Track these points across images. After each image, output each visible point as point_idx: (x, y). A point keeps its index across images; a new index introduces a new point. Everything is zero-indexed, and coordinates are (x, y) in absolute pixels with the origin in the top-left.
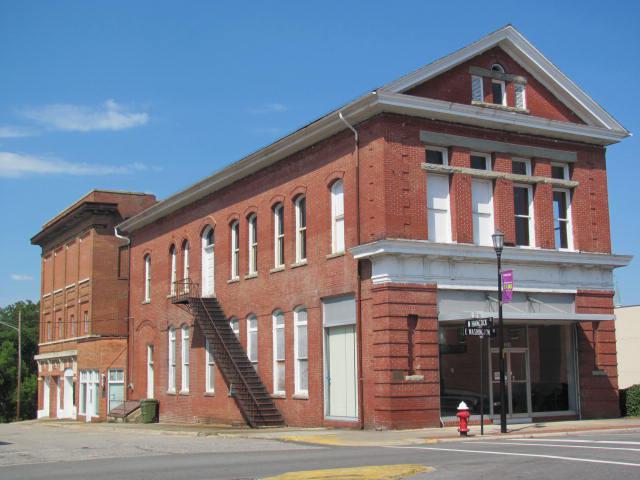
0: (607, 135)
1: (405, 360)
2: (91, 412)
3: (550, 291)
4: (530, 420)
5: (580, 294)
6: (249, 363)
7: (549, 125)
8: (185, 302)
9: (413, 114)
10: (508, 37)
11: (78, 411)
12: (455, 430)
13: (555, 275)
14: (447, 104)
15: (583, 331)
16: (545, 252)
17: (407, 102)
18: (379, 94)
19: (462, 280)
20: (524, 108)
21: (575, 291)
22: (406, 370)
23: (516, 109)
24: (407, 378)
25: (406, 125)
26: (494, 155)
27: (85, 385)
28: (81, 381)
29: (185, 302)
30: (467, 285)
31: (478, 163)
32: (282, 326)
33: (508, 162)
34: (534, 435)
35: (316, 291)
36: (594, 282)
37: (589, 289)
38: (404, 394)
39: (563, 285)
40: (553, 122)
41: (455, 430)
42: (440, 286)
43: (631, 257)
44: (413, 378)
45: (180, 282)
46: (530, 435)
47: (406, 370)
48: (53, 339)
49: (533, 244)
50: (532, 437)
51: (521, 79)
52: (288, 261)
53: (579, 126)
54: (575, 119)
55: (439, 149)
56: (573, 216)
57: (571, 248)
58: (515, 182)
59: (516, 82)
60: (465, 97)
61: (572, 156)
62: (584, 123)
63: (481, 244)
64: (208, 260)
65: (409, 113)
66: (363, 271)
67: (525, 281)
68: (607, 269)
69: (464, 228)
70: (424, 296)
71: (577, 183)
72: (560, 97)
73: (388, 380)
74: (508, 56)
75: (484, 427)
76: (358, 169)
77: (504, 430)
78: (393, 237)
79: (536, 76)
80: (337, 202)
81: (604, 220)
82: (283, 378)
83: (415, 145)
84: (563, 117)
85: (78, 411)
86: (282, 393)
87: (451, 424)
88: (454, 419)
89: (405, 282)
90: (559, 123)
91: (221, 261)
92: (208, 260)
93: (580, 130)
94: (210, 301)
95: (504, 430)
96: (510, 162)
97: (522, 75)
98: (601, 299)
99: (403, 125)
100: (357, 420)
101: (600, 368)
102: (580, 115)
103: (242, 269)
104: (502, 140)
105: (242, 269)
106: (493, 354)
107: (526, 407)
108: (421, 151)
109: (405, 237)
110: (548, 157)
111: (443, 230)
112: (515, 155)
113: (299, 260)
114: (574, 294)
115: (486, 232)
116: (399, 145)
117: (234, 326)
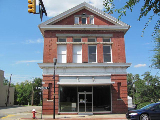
0: (122, 27)
1: (48, 96)
3: (101, 75)
4: (92, 114)
5: (112, 76)
6: (125, 104)
7: (99, 27)
9: (54, 30)
10: (86, 6)
13: (103, 70)
14: (62, 25)
15: (114, 87)
16: (99, 63)
17: (112, 27)
19: (68, 73)
20: (94, 23)
21: (111, 75)
22: (47, 99)
23: (92, 24)
24: (48, 100)
25: (52, 33)
26: (111, 37)
30: (69, 74)
31: (75, 40)
33: (87, 39)
37: (116, 74)
38: (46, 105)
39: (105, 73)
40: (100, 26)
42: (59, 75)
43: (131, 63)
44: (49, 101)
47: (47, 99)
49: (112, 62)
51: (92, 16)
53: (114, 26)
54: (113, 24)
55: (109, 38)
56: (112, 53)
57: (112, 62)
58: (88, 44)
59: (90, 17)
60: (72, 23)
61: (111, 35)
62: (115, 25)
63: (63, 63)
65: (53, 30)
67: (83, 73)
69: (70, 59)
71: (112, 43)
74: (87, 10)
75: (43, 115)
78: (45, 62)
81: (124, 53)
83: (54, 38)
84: (107, 24)
89: (48, 74)
90: (105, 26)
93: (111, 27)
96: (102, 39)
97: (93, 15)
98: (122, 77)
99: (51, 33)
101: (121, 98)
102: (114, 23)
104: (84, 33)
107: (92, 110)
108: (56, 39)
109: (49, 62)
110: (72, 36)
111: (64, 60)
112: (103, 37)
114: (110, 76)
115: (79, 60)
116: (49, 38)
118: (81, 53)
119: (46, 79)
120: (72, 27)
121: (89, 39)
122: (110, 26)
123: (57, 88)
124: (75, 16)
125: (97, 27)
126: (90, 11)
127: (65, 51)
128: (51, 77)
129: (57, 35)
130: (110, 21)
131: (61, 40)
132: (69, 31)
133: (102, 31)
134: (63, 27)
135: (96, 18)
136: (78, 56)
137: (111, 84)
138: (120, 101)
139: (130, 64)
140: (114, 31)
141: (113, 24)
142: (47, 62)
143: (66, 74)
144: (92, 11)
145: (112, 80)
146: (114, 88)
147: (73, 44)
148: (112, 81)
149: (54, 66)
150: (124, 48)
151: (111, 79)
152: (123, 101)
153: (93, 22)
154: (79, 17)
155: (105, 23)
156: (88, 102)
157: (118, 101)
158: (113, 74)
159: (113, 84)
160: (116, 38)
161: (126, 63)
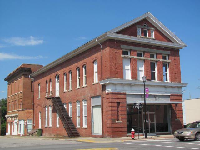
1: (116, 116)
2: (22, 133)
3: (162, 94)
5: (171, 95)
8: (50, 98)
10: (149, 16)
11: (18, 133)
12: (130, 138)
13: (164, 89)
14: (129, 36)
19: (134, 91)
20: (154, 38)
21: (170, 95)
22: (116, 119)
23: (151, 38)
24: (117, 121)
26: (144, 52)
34: (155, 139)
36: (176, 92)
39: (166, 92)
40: (163, 42)
41: (130, 138)
42: (127, 93)
45: (49, 92)
48: (11, 110)
51: (153, 29)
53: (171, 43)
54: (170, 41)
55: (127, 51)
57: (169, 81)
58: (151, 60)
59: (151, 30)
60: (135, 34)
61: (169, 53)
62: (173, 42)
64: (57, 85)
68: (180, 88)
69: (135, 75)
70: (122, 96)
71: (170, 61)
74: (148, 21)
79: (157, 28)
85: (18, 133)
86: (79, 126)
88: (131, 134)
89: (116, 92)
91: (61, 86)
95: (146, 138)
101: (178, 118)
102: (171, 40)
104: (147, 48)
108: (121, 51)
109: (116, 78)
111: (128, 75)
114: (169, 96)
118: (144, 70)
119: (114, 97)
120: (139, 39)
121: (150, 55)
122: (169, 43)
123: (125, 107)
124: (137, 26)
125: (158, 43)
126: (151, 22)
127: (129, 65)
128: (118, 95)
129: (122, 46)
130: (169, 38)
131: (125, 53)
132: (158, 47)
133: (162, 47)
134: (161, 43)
135: (156, 32)
136: (126, 71)
137: (170, 105)
138: (178, 121)
139: (186, 85)
140: (133, 42)
141: (170, 41)
142: (114, 78)
143: (133, 92)
144: (152, 23)
145: (171, 100)
146: (173, 108)
147: (138, 59)
148: (171, 101)
149: (143, 84)
150: (180, 68)
151: (169, 99)
152: (180, 121)
153: (153, 36)
154: (141, 28)
155: (164, 39)
156: (151, 122)
157: (176, 121)
158: (172, 94)
159: (172, 105)
160: (173, 56)
161: (180, 82)
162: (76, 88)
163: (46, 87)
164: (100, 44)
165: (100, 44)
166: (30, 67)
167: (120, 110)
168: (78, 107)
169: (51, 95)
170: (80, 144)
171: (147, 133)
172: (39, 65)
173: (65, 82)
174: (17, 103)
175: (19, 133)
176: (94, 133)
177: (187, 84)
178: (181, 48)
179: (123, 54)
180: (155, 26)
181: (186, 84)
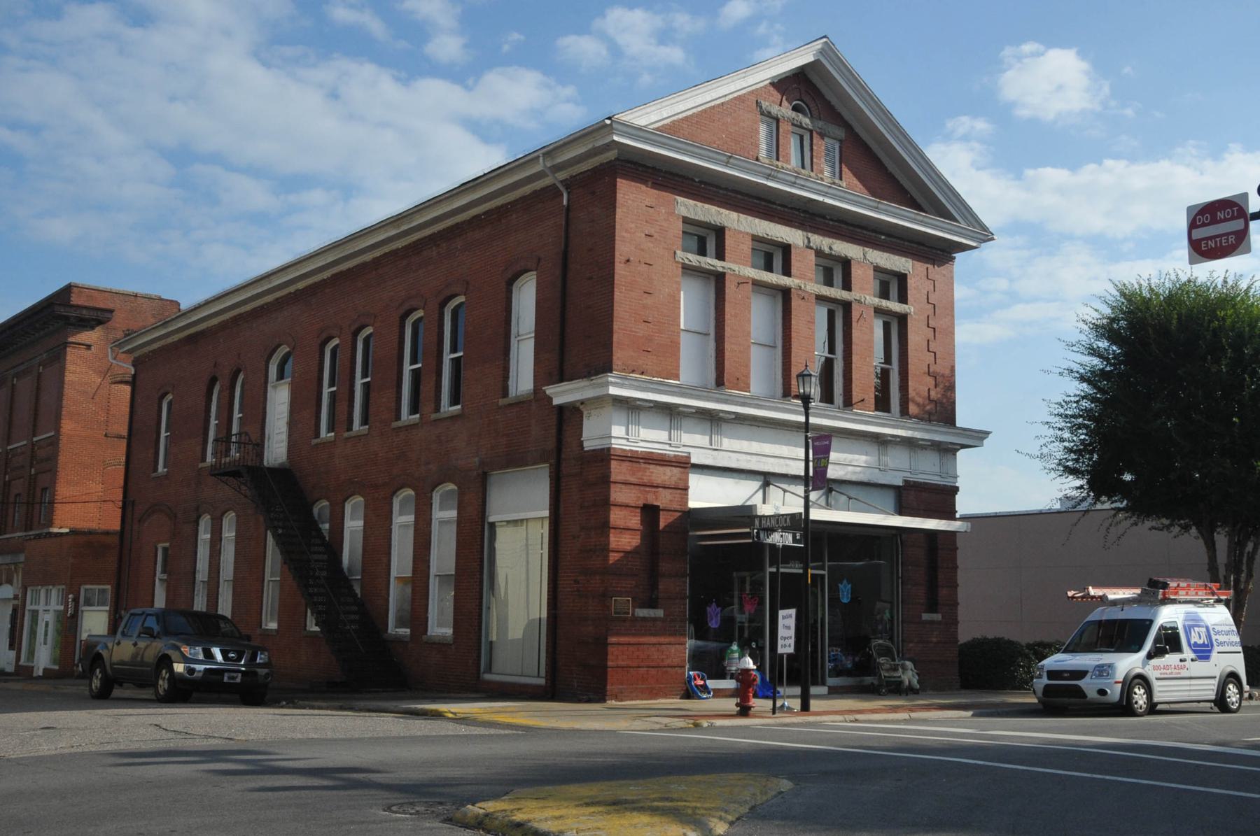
2: (43, 658)
8: (235, 474)
11: (18, 658)
12: (731, 704)
18: (615, 126)
27: (35, 614)
28: (28, 607)
29: (235, 474)
32: (410, 518)
34: (859, 717)
35: (476, 459)
36: (926, 470)
41: (731, 704)
45: (224, 440)
46: (852, 717)
48: (28, 527)
50: (856, 721)
52: (427, 407)
64: (279, 400)
66: (760, 347)
68: (948, 451)
70: (666, 475)
72: (892, 168)
73: (55, 505)
76: (566, 256)
77: (805, 707)
79: (858, 129)
80: (526, 299)
82: (407, 607)
85: (18, 658)
86: (406, 631)
87: (719, 693)
88: (729, 684)
91: (304, 405)
92: (279, 400)
94: (282, 474)
95: (805, 707)
100: (542, 681)
103: (340, 421)
105: (340, 421)
106: (770, 573)
113: (447, 408)
117: (321, 507)
162: (395, 424)
163: (208, 410)
164: (562, 188)
165: (562, 188)
166: (110, 306)
167: (200, 579)
168: (404, 526)
169: (234, 453)
170: (414, 740)
171: (814, 690)
172: (160, 299)
173: (163, 434)
174: (18, 495)
175: (22, 662)
176: (497, 666)
177: (987, 433)
178: (964, 248)
179: (683, 250)
180: (846, 115)
181: (977, 437)
